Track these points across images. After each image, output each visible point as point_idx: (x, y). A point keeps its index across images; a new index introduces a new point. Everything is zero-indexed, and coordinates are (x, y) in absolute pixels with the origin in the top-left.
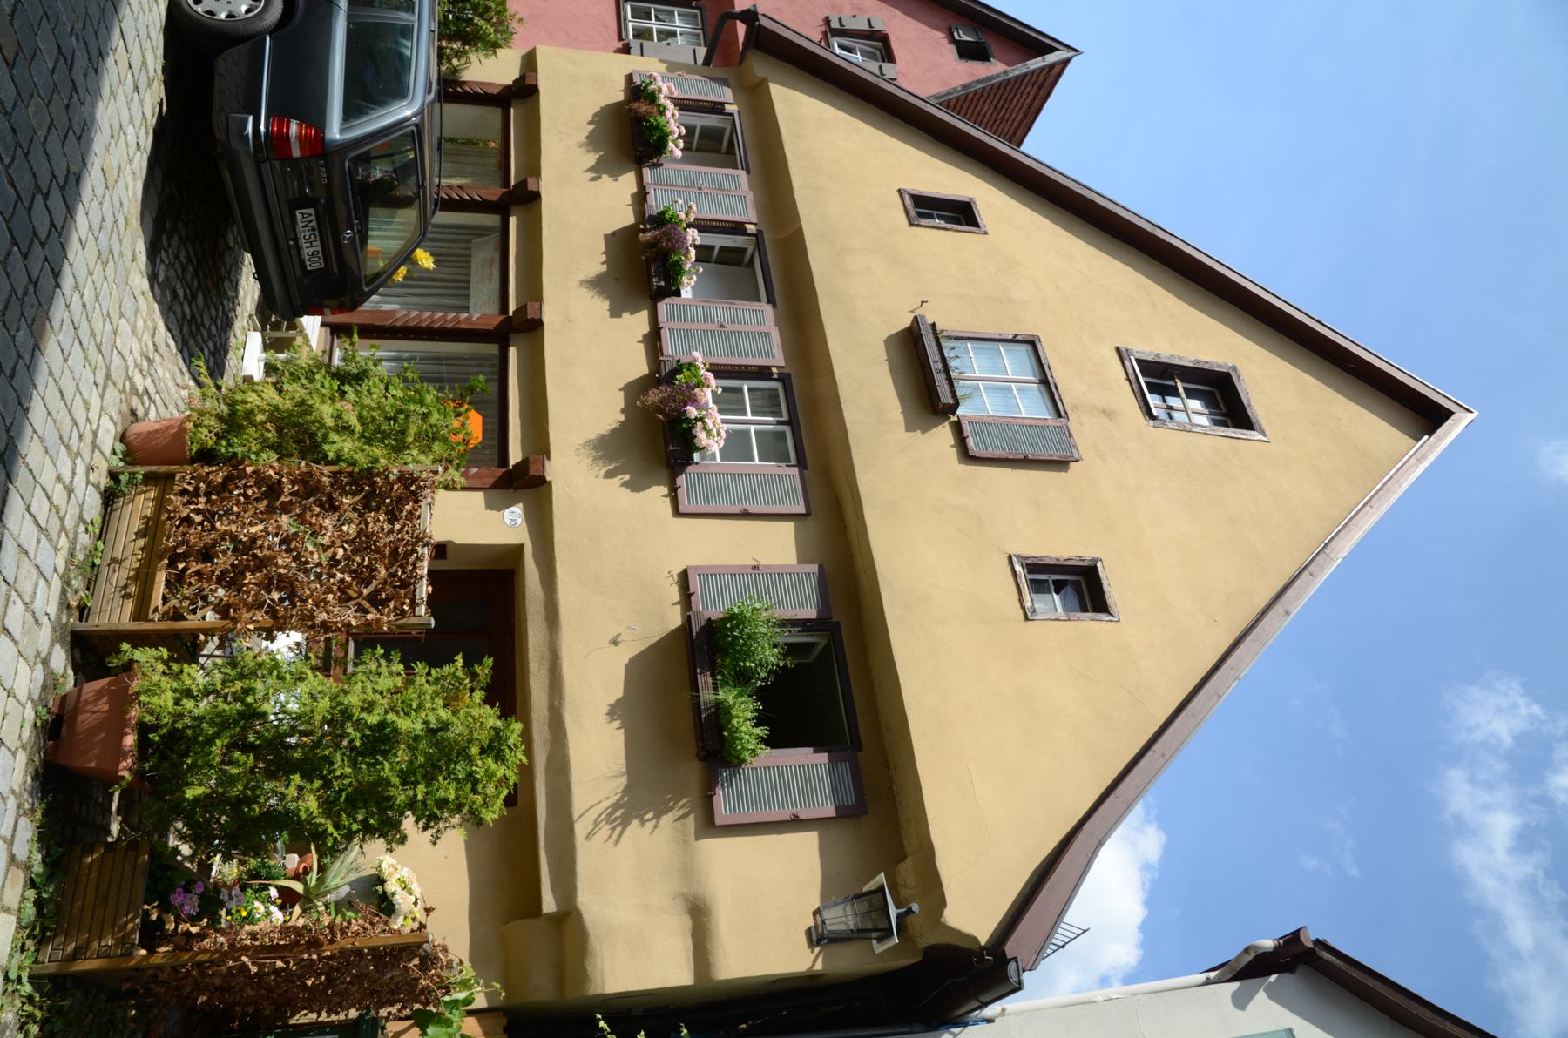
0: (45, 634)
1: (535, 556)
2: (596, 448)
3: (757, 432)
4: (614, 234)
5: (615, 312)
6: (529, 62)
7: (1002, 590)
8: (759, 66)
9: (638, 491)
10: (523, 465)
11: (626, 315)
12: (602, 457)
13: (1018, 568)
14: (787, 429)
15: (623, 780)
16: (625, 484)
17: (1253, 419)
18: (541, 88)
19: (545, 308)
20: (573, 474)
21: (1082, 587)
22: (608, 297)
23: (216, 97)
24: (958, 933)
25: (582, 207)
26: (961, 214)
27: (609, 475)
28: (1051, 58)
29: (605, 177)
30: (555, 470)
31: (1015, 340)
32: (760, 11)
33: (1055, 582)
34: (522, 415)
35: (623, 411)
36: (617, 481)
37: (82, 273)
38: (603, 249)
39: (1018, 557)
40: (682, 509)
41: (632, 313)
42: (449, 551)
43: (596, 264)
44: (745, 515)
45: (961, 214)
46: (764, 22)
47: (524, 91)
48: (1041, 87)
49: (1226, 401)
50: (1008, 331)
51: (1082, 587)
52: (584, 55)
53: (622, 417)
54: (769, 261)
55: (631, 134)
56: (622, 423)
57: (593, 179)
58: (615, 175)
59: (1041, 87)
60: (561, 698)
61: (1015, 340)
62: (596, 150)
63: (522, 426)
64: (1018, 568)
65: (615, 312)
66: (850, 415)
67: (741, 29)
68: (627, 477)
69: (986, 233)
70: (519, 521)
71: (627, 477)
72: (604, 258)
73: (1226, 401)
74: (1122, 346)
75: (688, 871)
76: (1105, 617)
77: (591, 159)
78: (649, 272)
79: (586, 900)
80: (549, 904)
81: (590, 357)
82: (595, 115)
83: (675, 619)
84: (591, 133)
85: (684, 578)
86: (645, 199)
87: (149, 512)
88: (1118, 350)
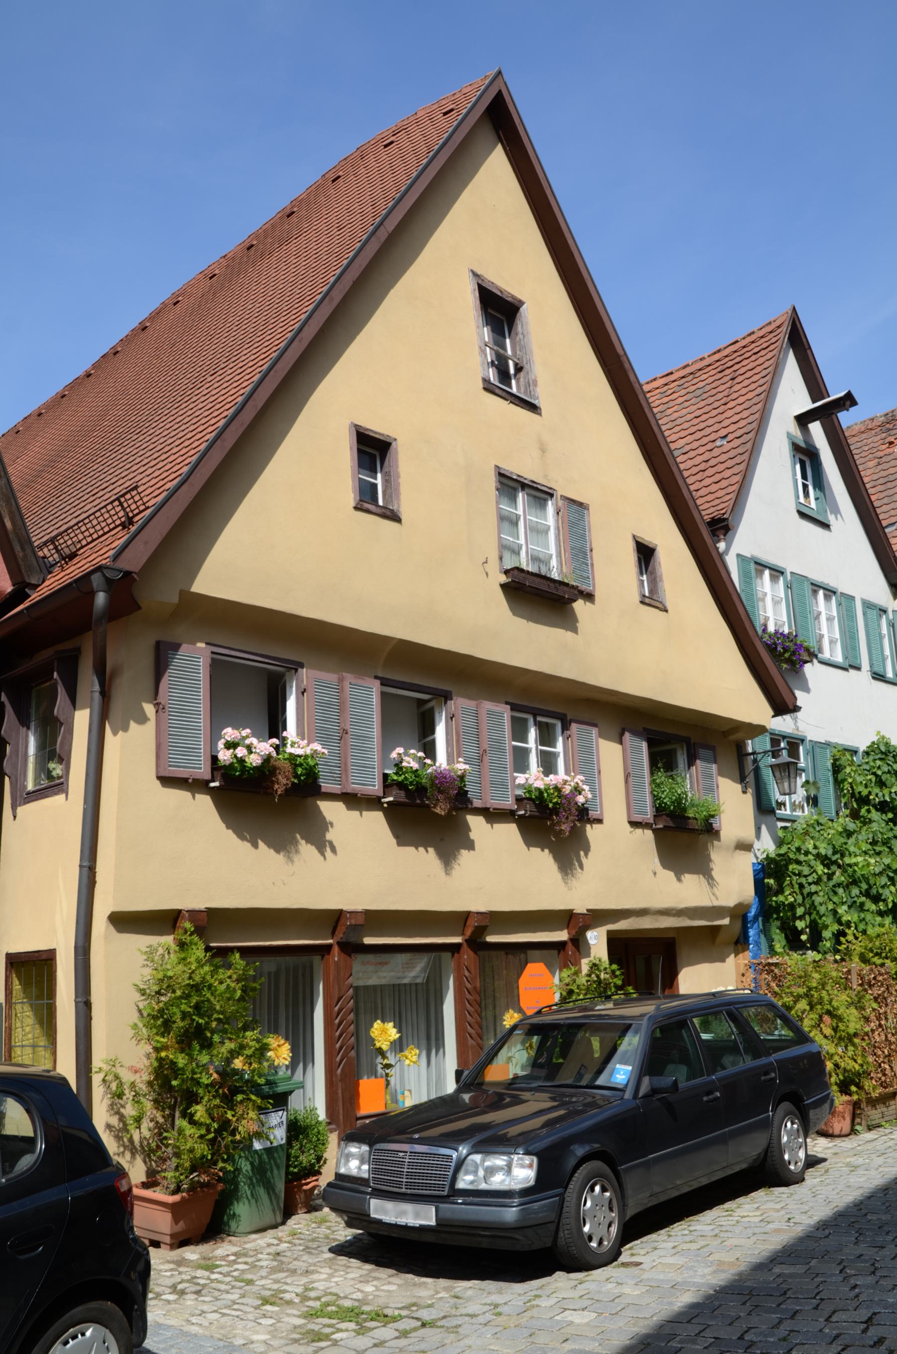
0: (381, 1301)
1: (614, 923)
2: (567, 874)
4: (396, 836)
5: (470, 845)
9: (589, 847)
11: (712, 865)
12: (571, 870)
15: (701, 876)
16: (586, 855)
19: (473, 909)
20: (581, 893)
22: (459, 851)
23: (380, 1233)
27: (581, 867)
29: (329, 836)
30: (580, 907)
34: (535, 931)
35: (543, 850)
36: (584, 860)
37: (739, 1212)
38: (412, 849)
41: (470, 831)
43: (426, 858)
53: (547, 851)
55: (267, 801)
56: (550, 851)
57: (334, 850)
58: (324, 825)
60: (673, 909)
62: (296, 843)
63: (542, 931)
65: (470, 845)
68: (582, 853)
70: (595, 933)
71: (582, 853)
72: (421, 849)
77: (307, 850)
78: (418, 806)
82: (241, 837)
83: (649, 833)
84: (269, 845)
86: (355, 795)
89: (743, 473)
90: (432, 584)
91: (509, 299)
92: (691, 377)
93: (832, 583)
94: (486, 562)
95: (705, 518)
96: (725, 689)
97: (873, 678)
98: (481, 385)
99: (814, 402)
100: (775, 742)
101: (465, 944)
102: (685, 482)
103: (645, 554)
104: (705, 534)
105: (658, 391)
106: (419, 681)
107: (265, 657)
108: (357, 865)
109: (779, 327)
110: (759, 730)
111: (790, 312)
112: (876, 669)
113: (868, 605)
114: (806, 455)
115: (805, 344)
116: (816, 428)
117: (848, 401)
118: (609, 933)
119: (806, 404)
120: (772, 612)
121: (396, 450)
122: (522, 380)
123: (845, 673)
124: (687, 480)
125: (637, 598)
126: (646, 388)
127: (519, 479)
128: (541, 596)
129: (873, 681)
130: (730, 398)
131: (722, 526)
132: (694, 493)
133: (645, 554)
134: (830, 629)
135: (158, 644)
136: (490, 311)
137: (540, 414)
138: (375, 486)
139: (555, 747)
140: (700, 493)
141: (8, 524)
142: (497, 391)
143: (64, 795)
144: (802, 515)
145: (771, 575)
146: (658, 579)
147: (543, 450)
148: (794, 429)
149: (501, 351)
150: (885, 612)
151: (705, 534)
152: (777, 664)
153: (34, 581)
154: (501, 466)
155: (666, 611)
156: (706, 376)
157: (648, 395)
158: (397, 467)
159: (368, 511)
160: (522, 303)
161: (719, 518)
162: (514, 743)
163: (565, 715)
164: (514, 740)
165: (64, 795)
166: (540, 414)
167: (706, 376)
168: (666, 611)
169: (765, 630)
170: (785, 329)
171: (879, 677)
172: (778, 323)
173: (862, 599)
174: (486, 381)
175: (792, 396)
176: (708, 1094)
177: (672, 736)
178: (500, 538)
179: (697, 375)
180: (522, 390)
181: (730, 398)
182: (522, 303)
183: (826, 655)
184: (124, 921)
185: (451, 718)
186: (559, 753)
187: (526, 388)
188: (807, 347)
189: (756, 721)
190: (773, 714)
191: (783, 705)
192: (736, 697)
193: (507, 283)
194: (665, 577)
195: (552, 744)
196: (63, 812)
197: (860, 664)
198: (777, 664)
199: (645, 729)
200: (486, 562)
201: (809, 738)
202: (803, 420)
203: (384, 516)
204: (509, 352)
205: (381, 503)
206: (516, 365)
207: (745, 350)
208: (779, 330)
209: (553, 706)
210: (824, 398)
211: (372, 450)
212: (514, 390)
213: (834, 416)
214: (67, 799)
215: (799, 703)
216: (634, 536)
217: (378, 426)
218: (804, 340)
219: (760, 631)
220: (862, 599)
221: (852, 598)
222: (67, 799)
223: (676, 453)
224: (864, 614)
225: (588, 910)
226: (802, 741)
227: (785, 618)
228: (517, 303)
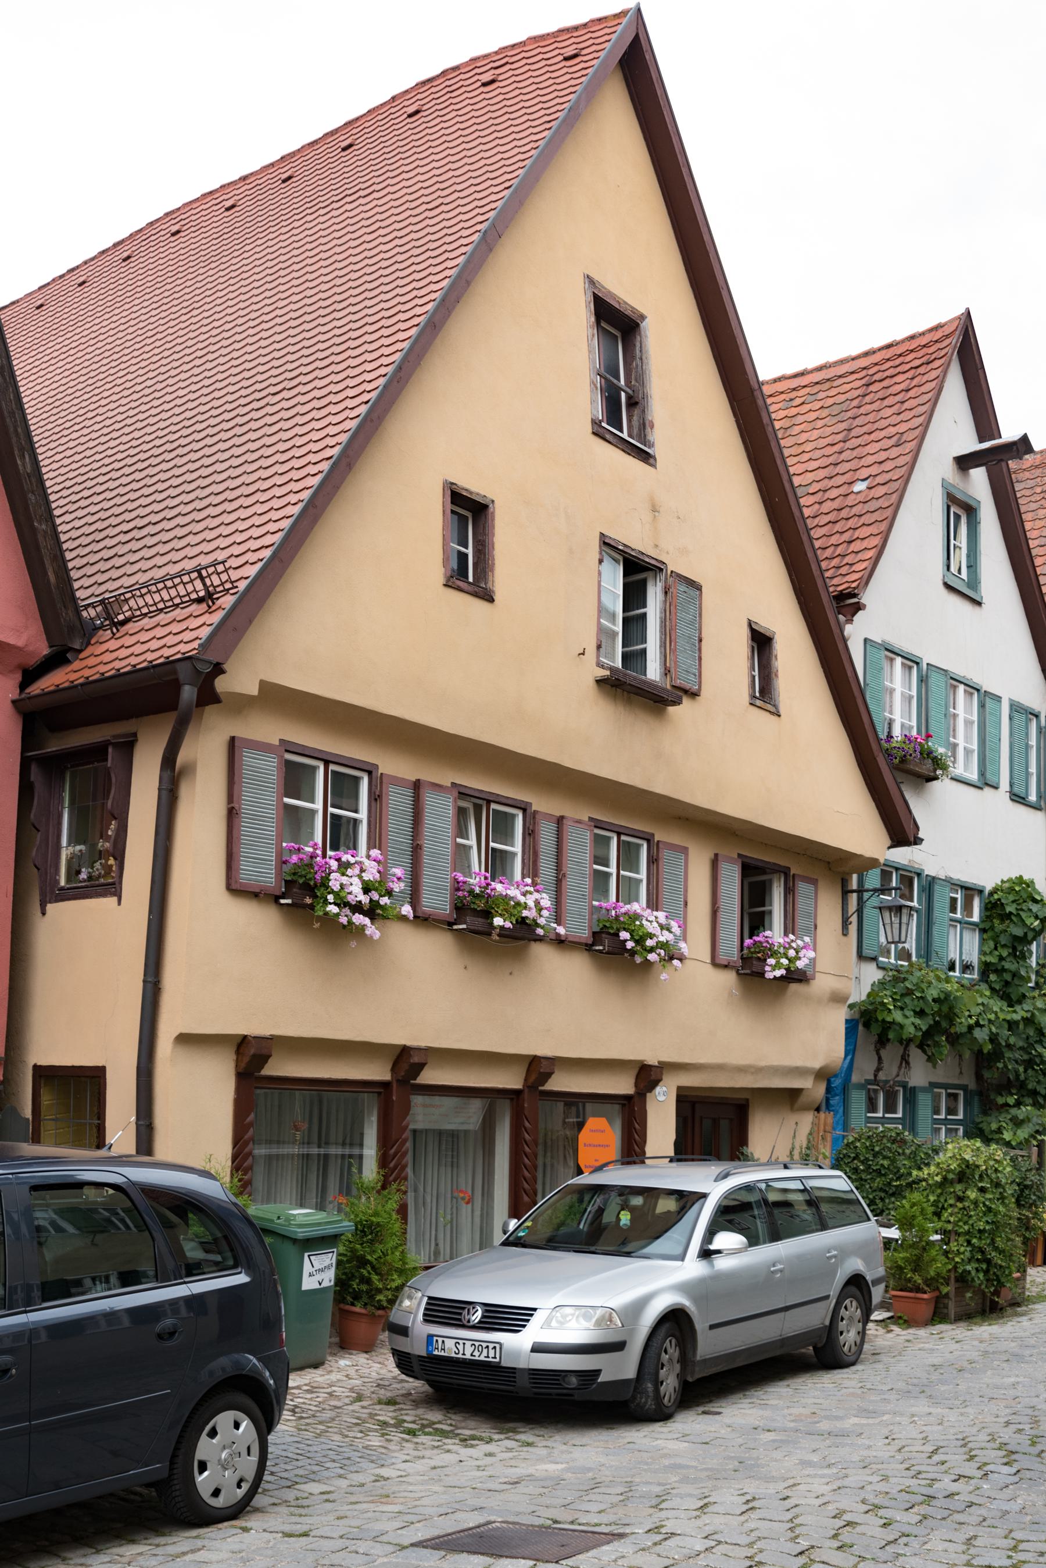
89: (884, 534)
90: (521, 674)
91: (628, 313)
92: (827, 385)
93: (977, 679)
94: (583, 654)
95: (831, 589)
96: (835, 811)
97: (1012, 800)
98: (589, 428)
99: (981, 441)
100: (886, 875)
101: (526, 1090)
102: (809, 535)
103: (761, 642)
104: (826, 607)
105: (783, 397)
106: (500, 786)
107: (343, 754)
108: (417, 996)
109: (947, 336)
110: (873, 863)
111: (963, 318)
112: (1016, 790)
113: (1016, 708)
114: (959, 508)
115: (978, 361)
116: (979, 475)
117: (1023, 446)
118: (679, 1088)
119: (970, 444)
120: (897, 714)
121: (493, 513)
122: (635, 418)
123: (980, 791)
124: (812, 533)
125: (746, 698)
126: (767, 390)
127: (626, 550)
128: (631, 690)
129: (1011, 803)
130: (876, 426)
131: (849, 603)
132: (819, 552)
133: (761, 642)
134: (968, 739)
135: (233, 739)
136: (603, 324)
137: (654, 466)
138: (466, 555)
139: (637, 872)
140: (828, 553)
141: (52, 578)
142: (608, 436)
143: (115, 899)
144: (948, 586)
145: (903, 664)
146: (773, 676)
147: (654, 510)
148: (948, 471)
149: (615, 381)
150: (1037, 716)
151: (826, 607)
152: (893, 773)
153: (77, 646)
154: (606, 533)
155: (779, 716)
156: (848, 387)
157: (769, 401)
158: (493, 535)
159: (459, 589)
160: (643, 317)
161: (849, 593)
162: (596, 867)
163: (653, 835)
164: (596, 863)
165: (115, 899)
166: (654, 466)
167: (848, 387)
168: (779, 716)
169: (890, 736)
170: (955, 340)
171: (1018, 798)
172: (947, 330)
173: (1010, 700)
174: (596, 423)
175: (952, 431)
176: (774, 1266)
177: (767, 868)
178: (599, 622)
179: (835, 384)
180: (635, 431)
181: (876, 426)
182: (643, 317)
183: (959, 770)
184: (185, 1040)
185: (376, 800)
186: (514, 854)
187: (640, 430)
188: (979, 366)
189: (868, 854)
190: (889, 843)
191: (901, 831)
192: (849, 823)
193: (627, 293)
194: (780, 674)
195: (635, 868)
196: (123, 917)
197: (998, 783)
198: (893, 773)
199: (739, 855)
200: (583, 654)
201: (926, 873)
202: (964, 463)
203: (475, 595)
204: (622, 382)
205: (471, 579)
206: (629, 398)
207: (901, 359)
208: (948, 341)
209: (646, 822)
210: (994, 439)
211: (468, 512)
212: (625, 435)
213: (1003, 464)
214: (119, 903)
215: (921, 835)
216: (750, 623)
217: (475, 485)
218: (977, 357)
219: (883, 735)
220: (1010, 700)
221: (998, 699)
222: (119, 903)
223: (800, 492)
224: (1011, 718)
225: (659, 1062)
226: (919, 875)
227: (914, 723)
228: (634, 317)
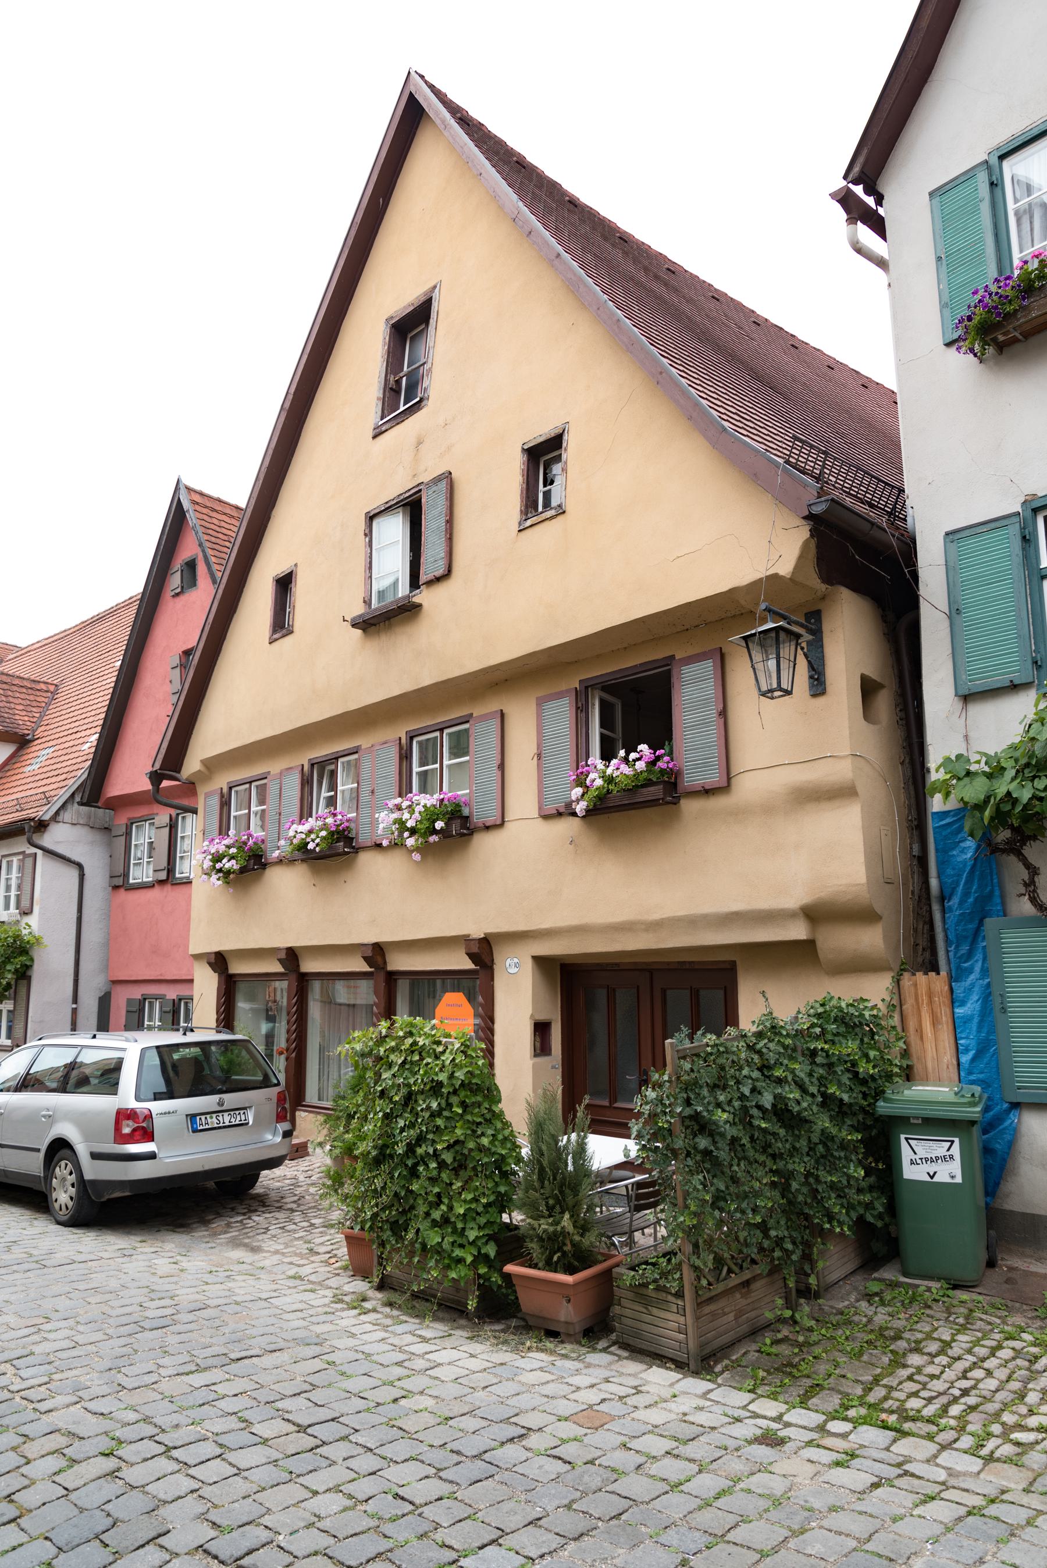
3: (420, 766)
6: (197, 957)
7: (547, 535)
8: (192, 765)
10: (472, 956)
13: (529, 523)
14: (446, 731)
17: (423, 299)
18: (217, 949)
21: (543, 455)
24: (801, 557)
25: (292, 913)
26: (284, 584)
28: (186, 504)
31: (369, 534)
32: (150, 769)
33: (545, 486)
39: (520, 524)
40: (498, 822)
42: (542, 1017)
44: (502, 767)
45: (284, 584)
46: (157, 766)
47: (219, 961)
48: (213, 510)
49: (411, 326)
50: (362, 540)
51: (543, 455)
52: (194, 914)
54: (318, 752)
59: (213, 510)
61: (369, 534)
64: (529, 523)
66: (427, 681)
67: (165, 783)
69: (296, 565)
73: (411, 326)
74: (371, 434)
75: (768, 809)
76: (565, 437)
79: (794, 900)
80: (798, 932)
81: (392, 905)
85: (546, 817)
87: (738, 1296)
88: (374, 437)
